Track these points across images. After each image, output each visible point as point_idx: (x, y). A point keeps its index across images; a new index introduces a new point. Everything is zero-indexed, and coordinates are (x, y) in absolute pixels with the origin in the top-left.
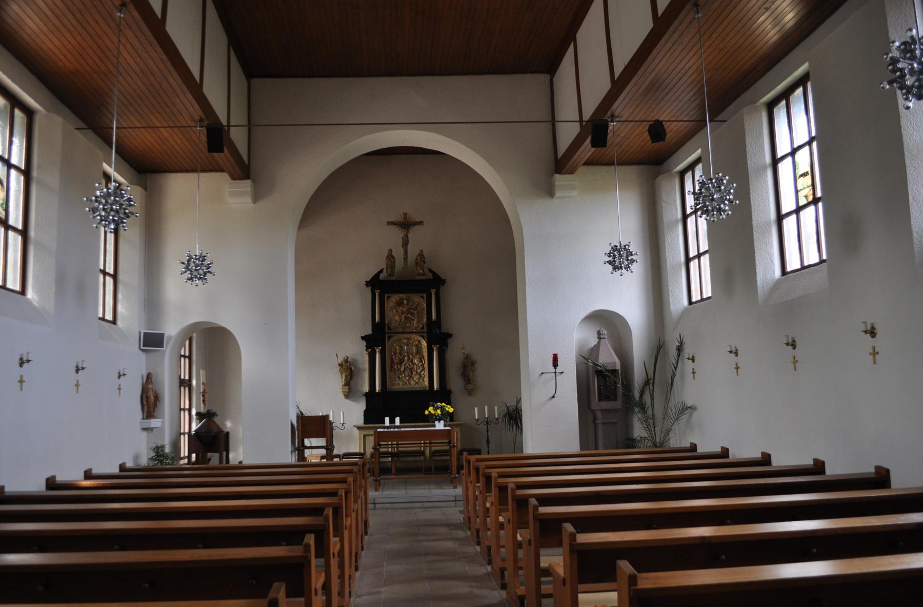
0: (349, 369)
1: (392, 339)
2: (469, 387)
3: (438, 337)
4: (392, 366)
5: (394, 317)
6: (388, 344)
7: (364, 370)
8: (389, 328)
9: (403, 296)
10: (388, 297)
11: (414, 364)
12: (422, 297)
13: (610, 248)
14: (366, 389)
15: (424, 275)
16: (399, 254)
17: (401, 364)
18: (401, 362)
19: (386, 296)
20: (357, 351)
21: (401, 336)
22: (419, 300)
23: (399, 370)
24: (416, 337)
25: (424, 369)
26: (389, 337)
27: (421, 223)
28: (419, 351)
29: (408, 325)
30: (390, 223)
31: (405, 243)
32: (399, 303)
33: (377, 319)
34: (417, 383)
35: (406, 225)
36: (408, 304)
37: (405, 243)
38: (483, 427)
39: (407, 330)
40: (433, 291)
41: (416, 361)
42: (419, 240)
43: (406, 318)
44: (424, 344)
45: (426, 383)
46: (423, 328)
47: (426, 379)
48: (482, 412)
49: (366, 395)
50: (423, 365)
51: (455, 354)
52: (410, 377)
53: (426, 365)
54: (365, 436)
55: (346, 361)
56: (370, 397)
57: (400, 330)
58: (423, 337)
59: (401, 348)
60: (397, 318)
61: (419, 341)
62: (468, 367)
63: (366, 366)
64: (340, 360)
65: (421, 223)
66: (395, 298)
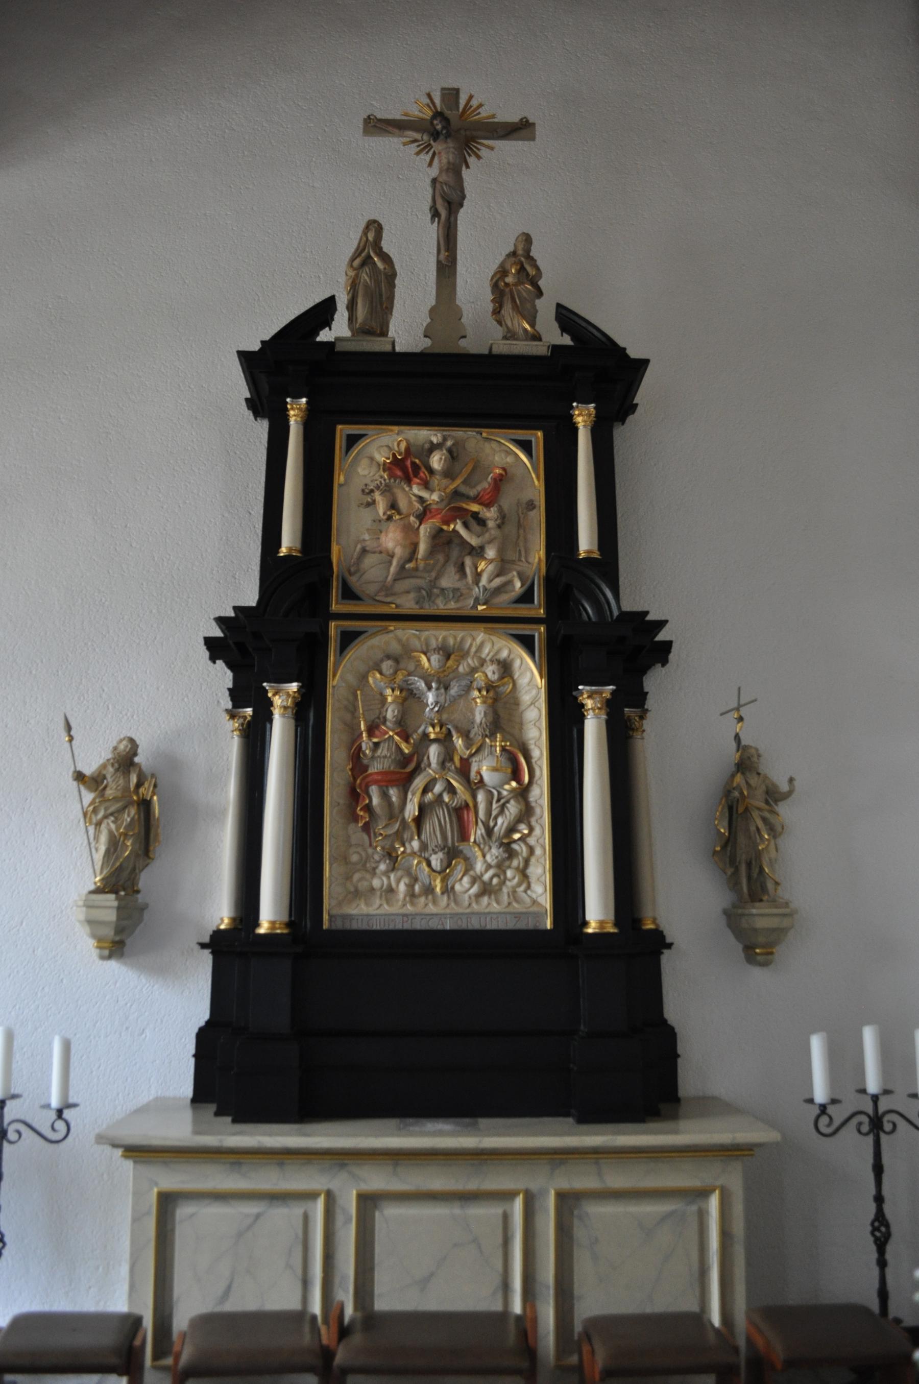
0: (134, 809)
1: (358, 652)
2: (761, 917)
3: (602, 646)
4: (355, 795)
5: (374, 534)
6: (340, 677)
7: (218, 815)
8: (349, 594)
9: (433, 435)
10: (352, 440)
11: (475, 786)
12: (526, 446)
13: (645, 727)
14: (221, 912)
15: (537, 337)
16: (412, 249)
17: (405, 782)
18: (405, 772)
19: (342, 431)
20: (182, 709)
21: (408, 633)
22: (510, 455)
23: (394, 813)
24: (499, 645)
25: (526, 814)
26: (348, 639)
27: (521, 129)
28: (503, 713)
29: (449, 580)
30: (376, 126)
31: (448, 204)
32: (407, 467)
33: (289, 540)
34: (487, 890)
35: (453, 131)
36: (448, 474)
37: (448, 204)
38: (854, 1150)
39: (442, 606)
40: (583, 417)
41: (486, 768)
42: (503, 201)
43: (443, 541)
44: (531, 680)
45: (541, 891)
46: (526, 597)
47: (541, 872)
48: (845, 1059)
49: (220, 945)
50: (523, 793)
51: (689, 727)
52: (452, 854)
53: (541, 795)
54: (167, 1202)
55: (126, 761)
56: (233, 949)
57: (408, 604)
58: (527, 642)
59: (409, 696)
60: (392, 539)
61: (506, 668)
62: (743, 821)
63: (230, 792)
64: (94, 756)
65: (521, 129)
66: (384, 443)
